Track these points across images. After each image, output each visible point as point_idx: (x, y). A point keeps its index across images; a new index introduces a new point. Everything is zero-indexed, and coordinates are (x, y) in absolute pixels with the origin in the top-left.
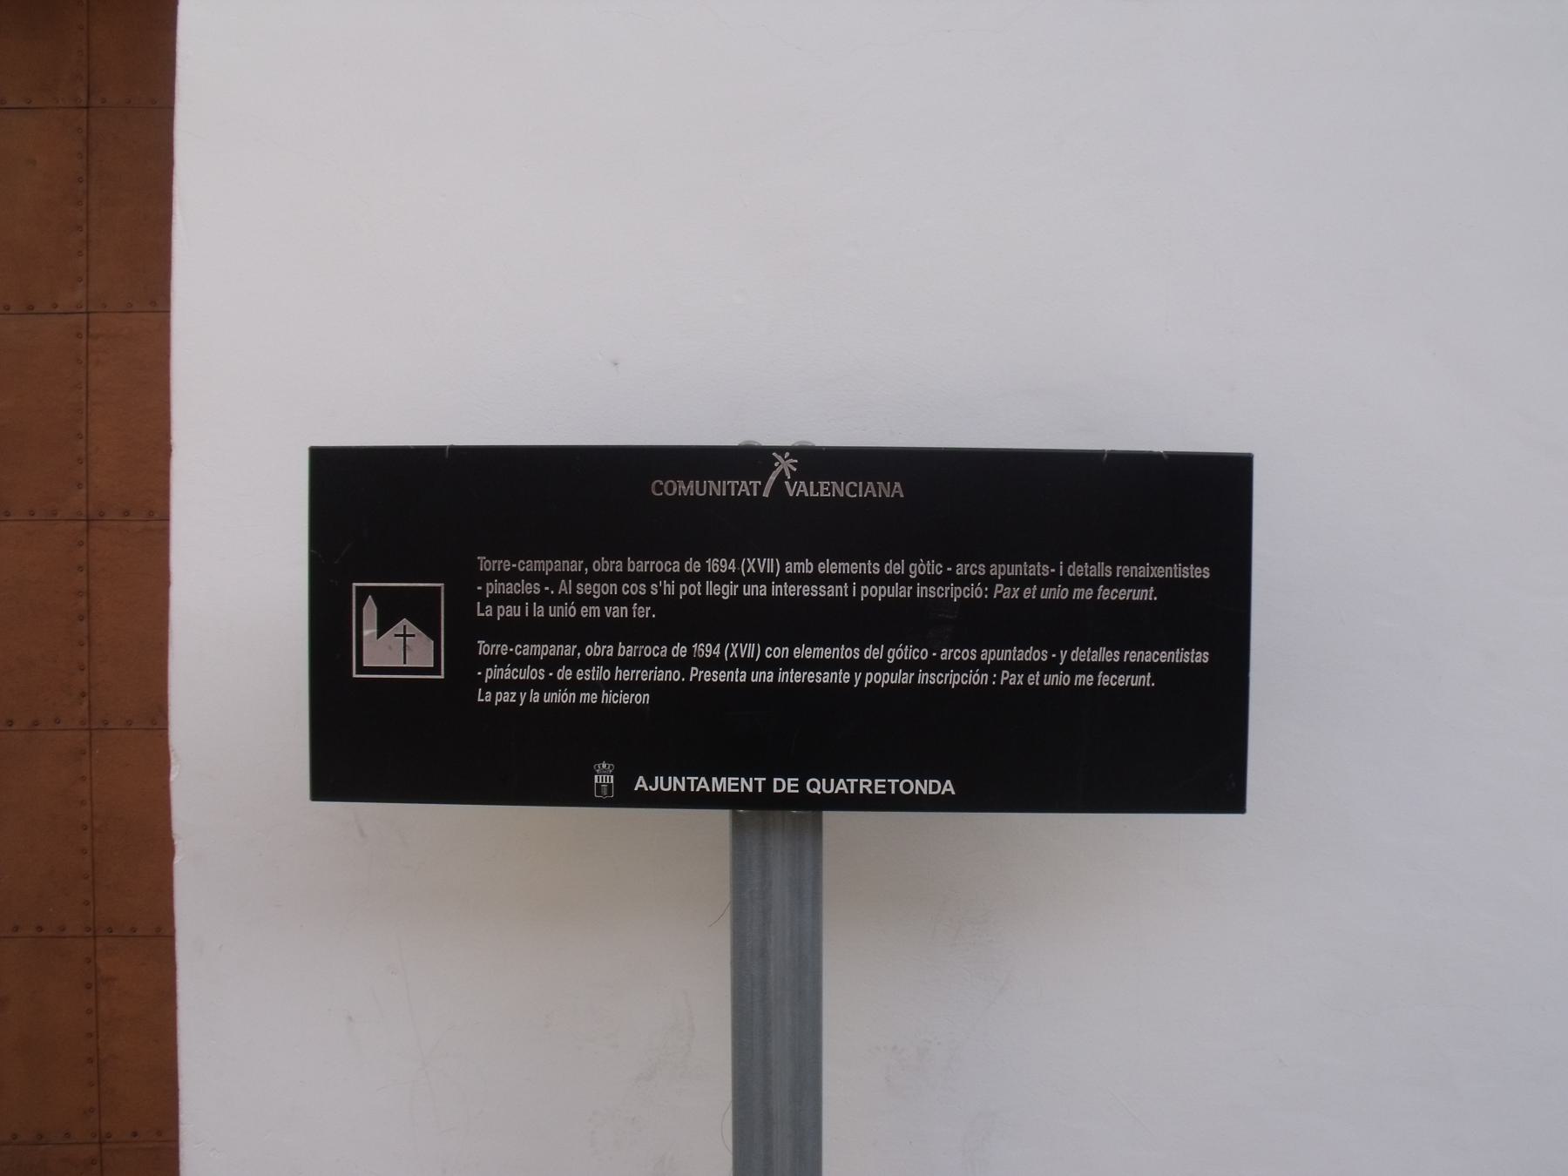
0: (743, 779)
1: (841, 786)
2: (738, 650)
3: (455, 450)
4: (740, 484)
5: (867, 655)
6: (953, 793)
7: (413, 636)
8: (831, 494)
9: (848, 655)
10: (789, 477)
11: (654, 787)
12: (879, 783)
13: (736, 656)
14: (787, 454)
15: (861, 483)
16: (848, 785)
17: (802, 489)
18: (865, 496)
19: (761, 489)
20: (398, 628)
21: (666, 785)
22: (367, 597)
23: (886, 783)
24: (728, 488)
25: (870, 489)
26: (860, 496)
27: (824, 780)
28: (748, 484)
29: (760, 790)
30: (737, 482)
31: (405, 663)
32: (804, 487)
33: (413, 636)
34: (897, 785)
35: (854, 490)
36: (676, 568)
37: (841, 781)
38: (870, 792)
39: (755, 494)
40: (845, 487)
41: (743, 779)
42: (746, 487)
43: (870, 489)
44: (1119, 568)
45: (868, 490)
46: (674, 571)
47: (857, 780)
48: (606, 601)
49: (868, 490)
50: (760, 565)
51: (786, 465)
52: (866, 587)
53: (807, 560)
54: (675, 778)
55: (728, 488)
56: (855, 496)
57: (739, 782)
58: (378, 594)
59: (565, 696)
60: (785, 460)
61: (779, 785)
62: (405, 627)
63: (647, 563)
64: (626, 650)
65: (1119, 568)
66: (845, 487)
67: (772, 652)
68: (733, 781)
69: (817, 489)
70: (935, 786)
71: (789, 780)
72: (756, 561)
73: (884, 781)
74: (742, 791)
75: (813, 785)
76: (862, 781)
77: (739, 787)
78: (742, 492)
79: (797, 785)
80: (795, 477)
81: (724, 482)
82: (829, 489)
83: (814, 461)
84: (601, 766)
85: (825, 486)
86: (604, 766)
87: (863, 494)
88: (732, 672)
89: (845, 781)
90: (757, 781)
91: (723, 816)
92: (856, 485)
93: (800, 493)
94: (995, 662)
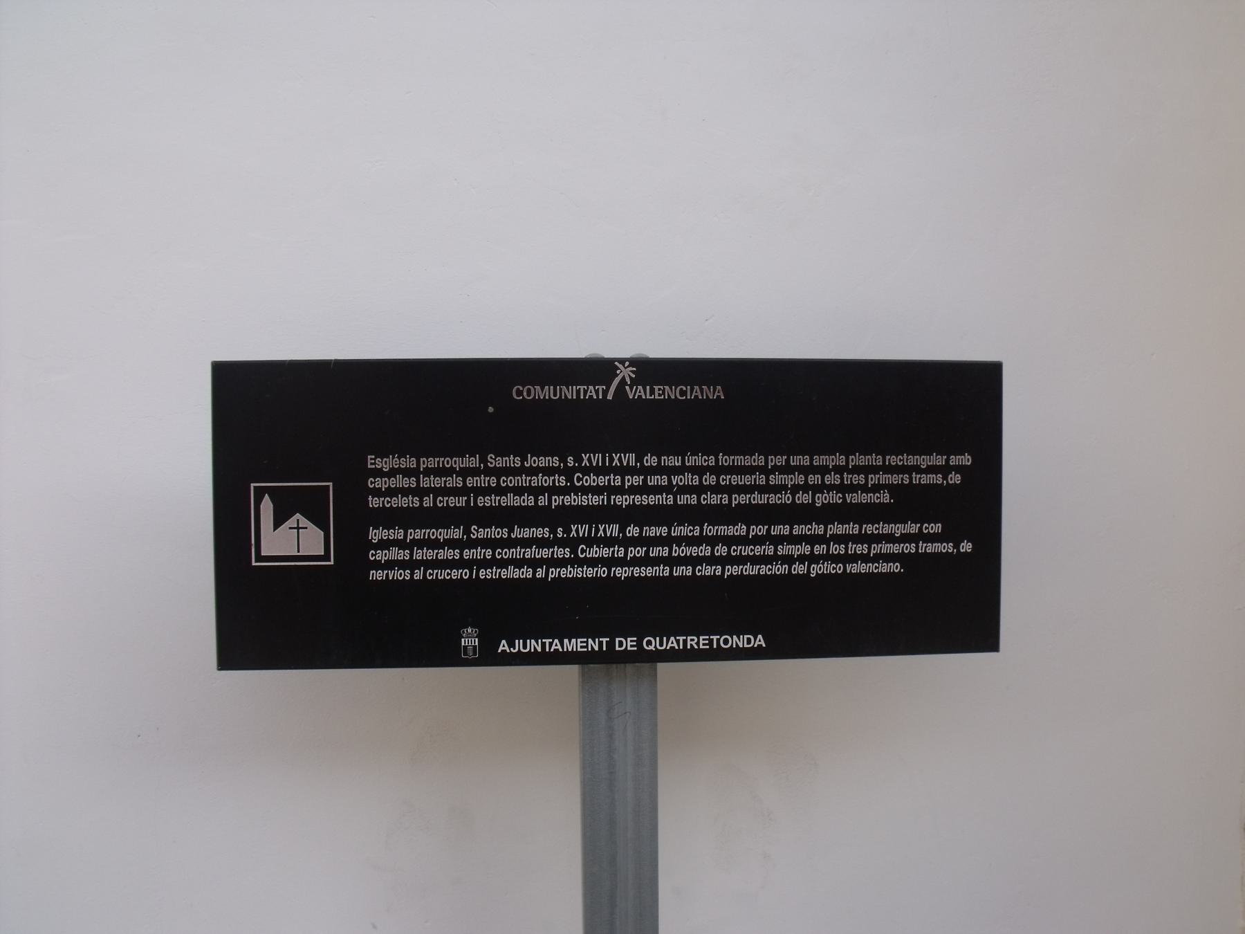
0: (590, 640)
1: (672, 643)
2: (604, 530)
3: (338, 363)
4: (588, 388)
5: (629, 533)
6: (764, 645)
7: (306, 528)
8: (664, 397)
9: (498, 534)
10: (629, 383)
11: (514, 649)
12: (704, 640)
13: (575, 536)
14: (627, 363)
15: (689, 387)
16: (678, 642)
17: (640, 392)
18: (715, 398)
19: (605, 393)
20: (292, 522)
21: (525, 647)
22: (264, 496)
23: (709, 639)
24: (578, 392)
25: (696, 392)
26: (689, 397)
27: (658, 639)
28: (594, 388)
29: (604, 649)
30: (586, 387)
31: (299, 552)
32: (642, 391)
33: (306, 528)
34: (718, 640)
35: (683, 393)
36: (712, 462)
37: (672, 639)
38: (696, 647)
39: (601, 397)
40: (535, 394)
41: (590, 640)
42: (593, 391)
43: (696, 392)
44: (888, 457)
45: (696, 393)
46: (710, 464)
47: (685, 638)
48: (795, 489)
49: (696, 393)
50: (592, 458)
51: (626, 373)
52: (629, 477)
53: (966, 454)
54: (533, 641)
55: (578, 392)
56: (684, 398)
57: (587, 642)
58: (274, 493)
59: (779, 568)
60: (626, 368)
61: (621, 644)
62: (298, 520)
63: (437, 459)
64: (415, 533)
65: (888, 457)
66: (535, 394)
67: (928, 528)
68: (581, 642)
69: (652, 392)
70: (749, 641)
71: (629, 639)
72: (590, 456)
73: (708, 637)
74: (590, 649)
75: (649, 643)
76: (689, 638)
77: (587, 647)
78: (590, 396)
79: (635, 643)
80: (634, 382)
81: (574, 387)
82: (661, 392)
83: (649, 370)
84: (467, 631)
85: (659, 389)
86: (469, 630)
87: (691, 396)
88: (514, 550)
89: (675, 639)
90: (545, 642)
91: (573, 670)
92: (685, 389)
93: (639, 396)
94: (381, 541)
